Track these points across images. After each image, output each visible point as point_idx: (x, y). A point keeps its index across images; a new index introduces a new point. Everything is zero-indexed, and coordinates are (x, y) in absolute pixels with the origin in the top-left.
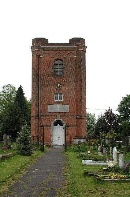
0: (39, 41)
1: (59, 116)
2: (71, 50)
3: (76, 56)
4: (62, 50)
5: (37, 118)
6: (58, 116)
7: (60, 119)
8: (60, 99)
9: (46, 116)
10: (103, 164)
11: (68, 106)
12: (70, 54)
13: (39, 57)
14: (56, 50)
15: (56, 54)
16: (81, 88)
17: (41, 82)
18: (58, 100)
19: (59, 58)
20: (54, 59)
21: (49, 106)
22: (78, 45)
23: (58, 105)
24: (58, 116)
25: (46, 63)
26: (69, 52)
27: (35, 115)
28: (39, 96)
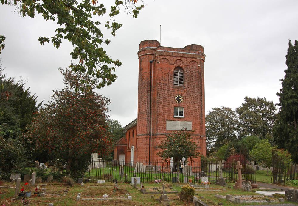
0: (151, 43)
2: (194, 58)
3: (200, 65)
4: (183, 57)
5: (149, 137)
8: (180, 115)
9: (164, 134)
11: (190, 123)
13: (153, 62)
14: (176, 56)
15: (176, 60)
18: (178, 116)
19: (179, 65)
20: (174, 67)
21: (168, 123)
22: (195, 53)
23: (179, 122)
25: (164, 70)
26: (177, 58)
27: (145, 133)
28: (150, 110)
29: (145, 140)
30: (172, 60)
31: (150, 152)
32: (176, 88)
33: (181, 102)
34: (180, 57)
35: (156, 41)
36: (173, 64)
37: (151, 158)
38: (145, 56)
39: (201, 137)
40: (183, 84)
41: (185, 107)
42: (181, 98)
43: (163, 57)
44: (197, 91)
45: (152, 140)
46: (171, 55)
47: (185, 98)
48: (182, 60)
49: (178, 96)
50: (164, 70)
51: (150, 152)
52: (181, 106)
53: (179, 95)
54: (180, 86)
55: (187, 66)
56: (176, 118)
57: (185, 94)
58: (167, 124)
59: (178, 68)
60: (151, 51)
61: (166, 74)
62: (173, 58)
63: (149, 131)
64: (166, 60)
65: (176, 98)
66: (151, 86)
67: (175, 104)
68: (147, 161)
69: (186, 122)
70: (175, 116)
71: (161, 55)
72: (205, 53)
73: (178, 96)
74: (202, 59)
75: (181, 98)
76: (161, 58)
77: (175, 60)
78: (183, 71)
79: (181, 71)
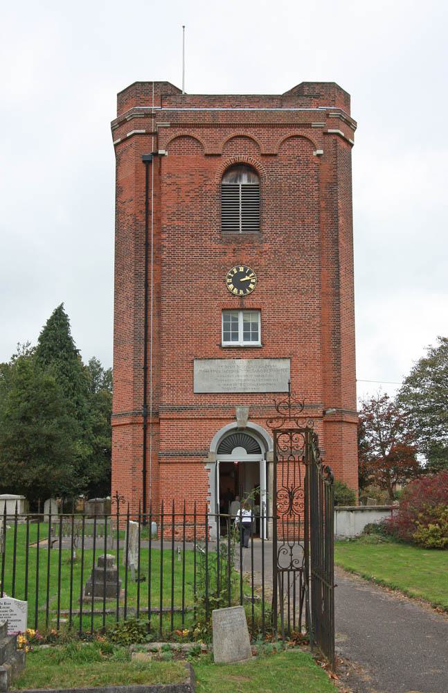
1: (246, 410)
3: (321, 152)
4: (255, 126)
5: (141, 419)
6: (242, 411)
7: (250, 425)
8: (246, 337)
10: (215, 527)
11: (285, 365)
12: (294, 143)
13: (151, 161)
16: (338, 294)
17: (159, 261)
18: (241, 342)
19: (243, 158)
20: (220, 165)
21: (199, 367)
22: (318, 118)
23: (242, 364)
24: (242, 411)
27: (129, 409)
28: (146, 327)
29: (129, 429)
30: (213, 141)
31: (145, 472)
32: (228, 242)
33: (250, 289)
34: (247, 126)
35: (166, 84)
36: (219, 155)
37: (150, 492)
38: (128, 144)
39: (324, 413)
40: (255, 224)
41: (266, 309)
42: (247, 278)
43: (178, 133)
44: (312, 249)
45: (151, 430)
46: (208, 120)
47: (262, 275)
48: (250, 139)
49: (238, 269)
50: (184, 179)
51: (145, 472)
52: (248, 306)
53: (242, 265)
54: (246, 232)
55: (273, 159)
56: (229, 348)
57: (263, 262)
58: (196, 373)
59: (239, 167)
60: (147, 120)
61: (192, 194)
62: (216, 132)
63: (142, 402)
64: (185, 144)
65: (230, 277)
66: (147, 245)
67: (226, 301)
68: (137, 502)
69: (267, 361)
70: (225, 344)
71: (173, 126)
72: (354, 115)
73: (238, 269)
74: (338, 134)
75: (247, 278)
76: (173, 136)
77: (225, 139)
78: (256, 178)
79: (249, 180)
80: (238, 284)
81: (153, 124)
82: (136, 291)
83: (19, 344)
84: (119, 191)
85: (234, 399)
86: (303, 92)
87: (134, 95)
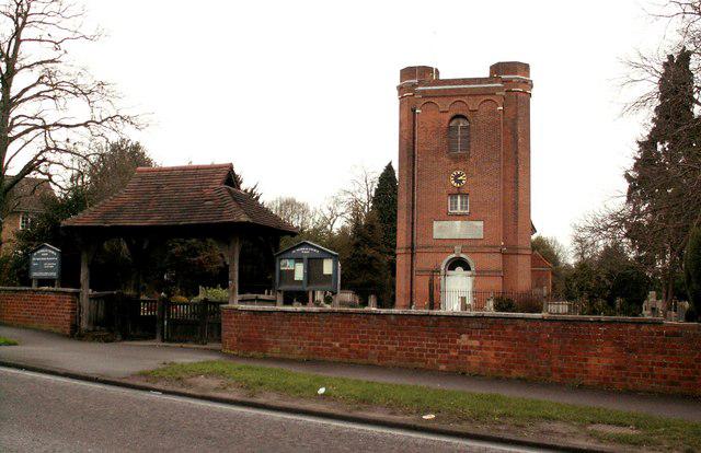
7: (462, 256)
8: (462, 208)
11: (480, 224)
20: (448, 117)
23: (458, 223)
30: (444, 104)
80: (457, 181)
81: (419, 88)
82: (406, 283)
83: (68, 140)
84: (401, 136)
85: (454, 242)
86: (498, 69)
87: (407, 73)
